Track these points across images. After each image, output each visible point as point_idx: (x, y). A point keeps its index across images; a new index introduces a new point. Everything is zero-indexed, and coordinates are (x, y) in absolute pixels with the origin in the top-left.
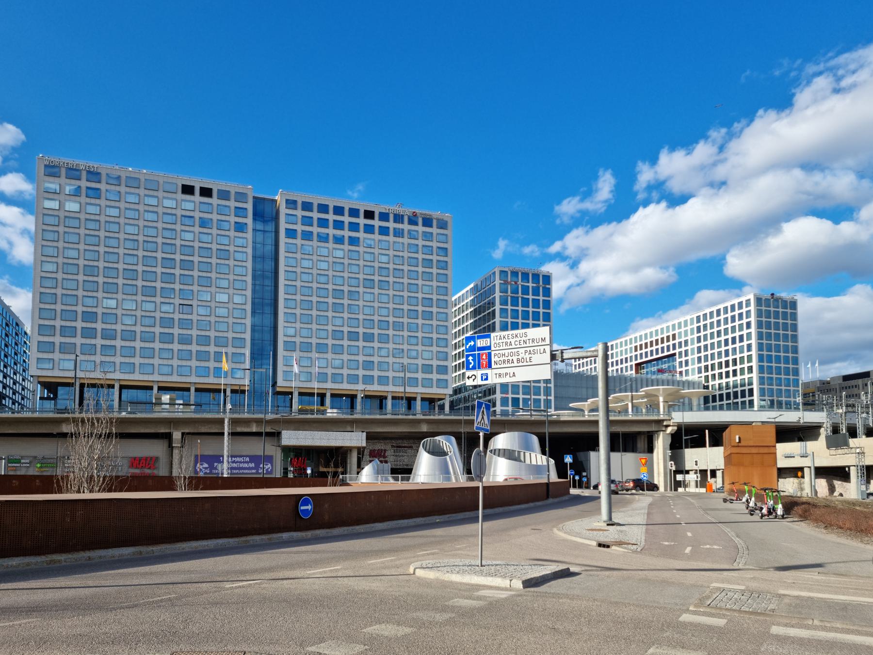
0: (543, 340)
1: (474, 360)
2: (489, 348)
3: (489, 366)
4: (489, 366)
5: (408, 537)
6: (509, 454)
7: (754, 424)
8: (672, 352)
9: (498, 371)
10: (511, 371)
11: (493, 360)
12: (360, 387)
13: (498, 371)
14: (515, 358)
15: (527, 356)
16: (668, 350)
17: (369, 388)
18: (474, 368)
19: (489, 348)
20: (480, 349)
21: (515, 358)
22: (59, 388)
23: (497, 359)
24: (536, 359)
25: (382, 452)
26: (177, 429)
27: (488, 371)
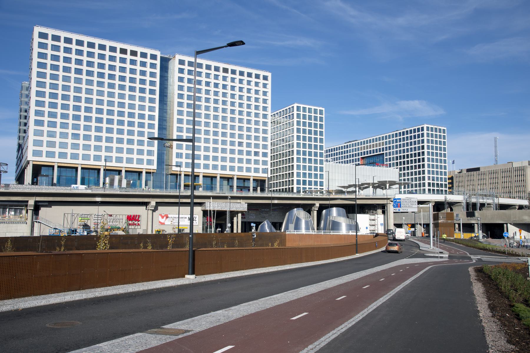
0: (416, 201)
1: (396, 205)
2: (400, 202)
3: (401, 207)
4: (401, 207)
5: (189, 270)
6: (297, 227)
7: (27, 214)
8: (382, 152)
9: (403, 209)
10: (407, 209)
11: (401, 205)
12: (103, 163)
13: (403, 209)
14: (408, 206)
15: (411, 205)
16: (380, 151)
17: (108, 164)
18: (396, 207)
19: (400, 202)
20: (398, 202)
21: (408, 206)
22: (43, 168)
23: (402, 205)
24: (414, 206)
25: (136, 217)
26: (153, 200)
27: (400, 208)
